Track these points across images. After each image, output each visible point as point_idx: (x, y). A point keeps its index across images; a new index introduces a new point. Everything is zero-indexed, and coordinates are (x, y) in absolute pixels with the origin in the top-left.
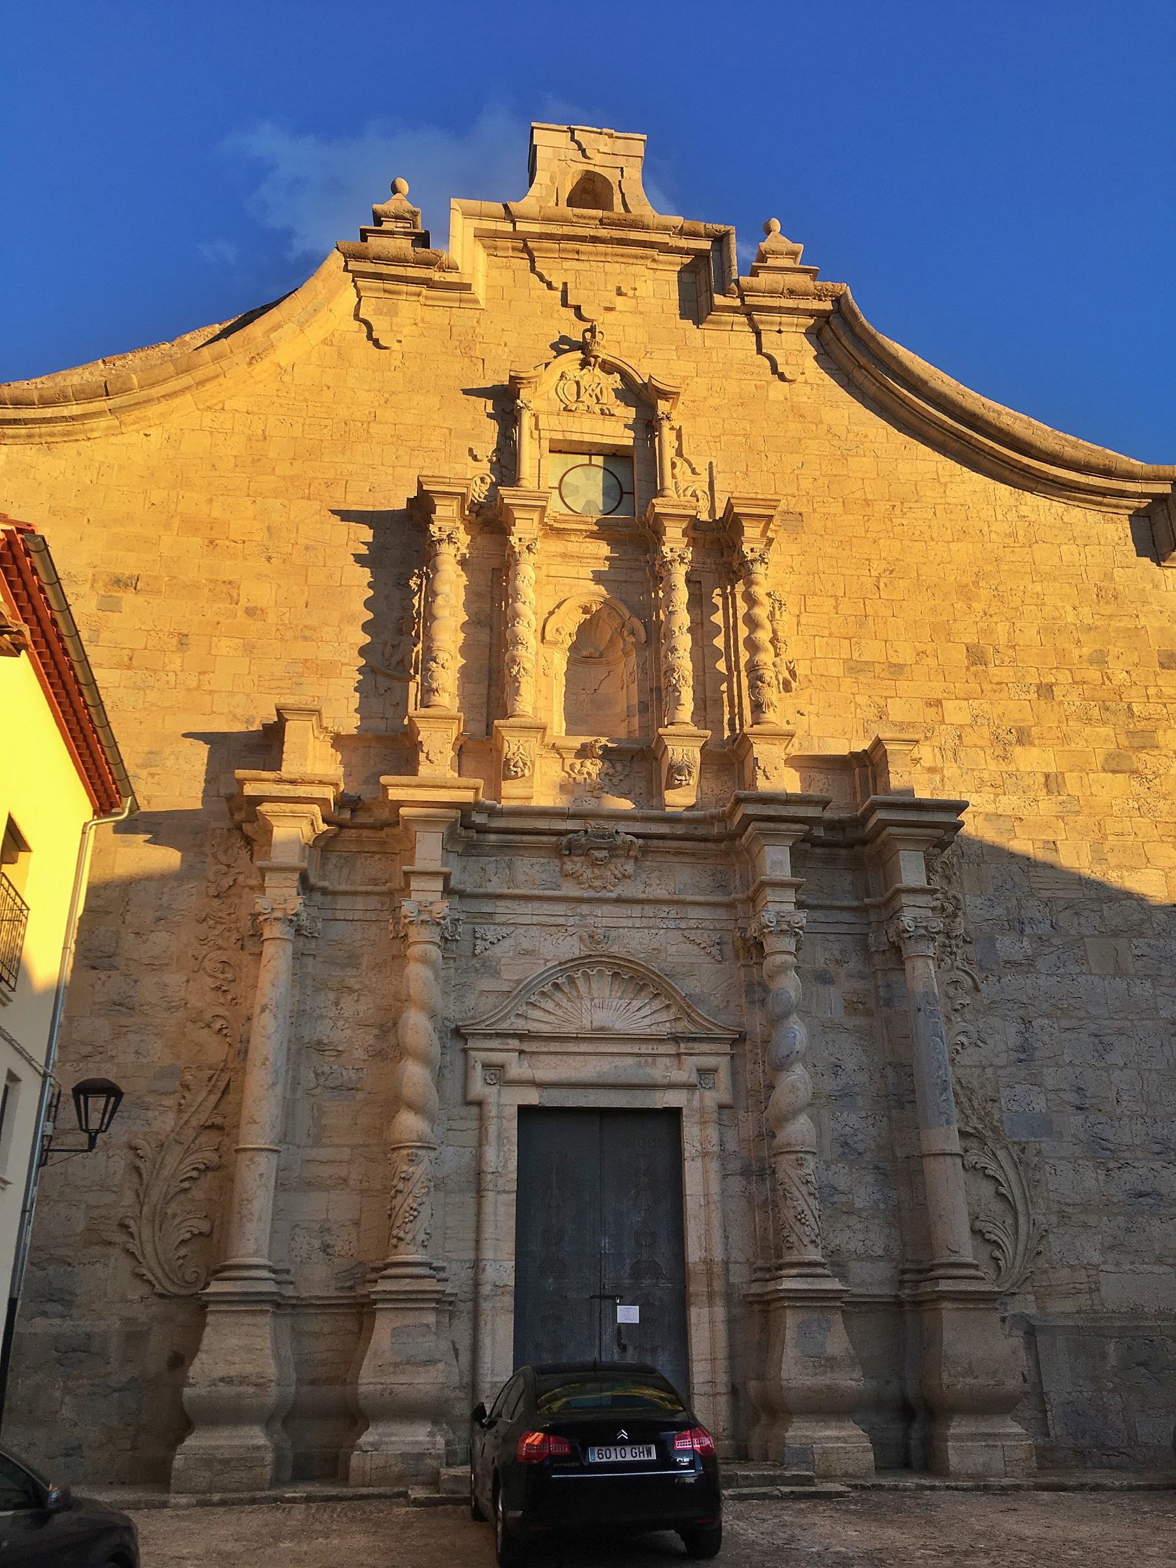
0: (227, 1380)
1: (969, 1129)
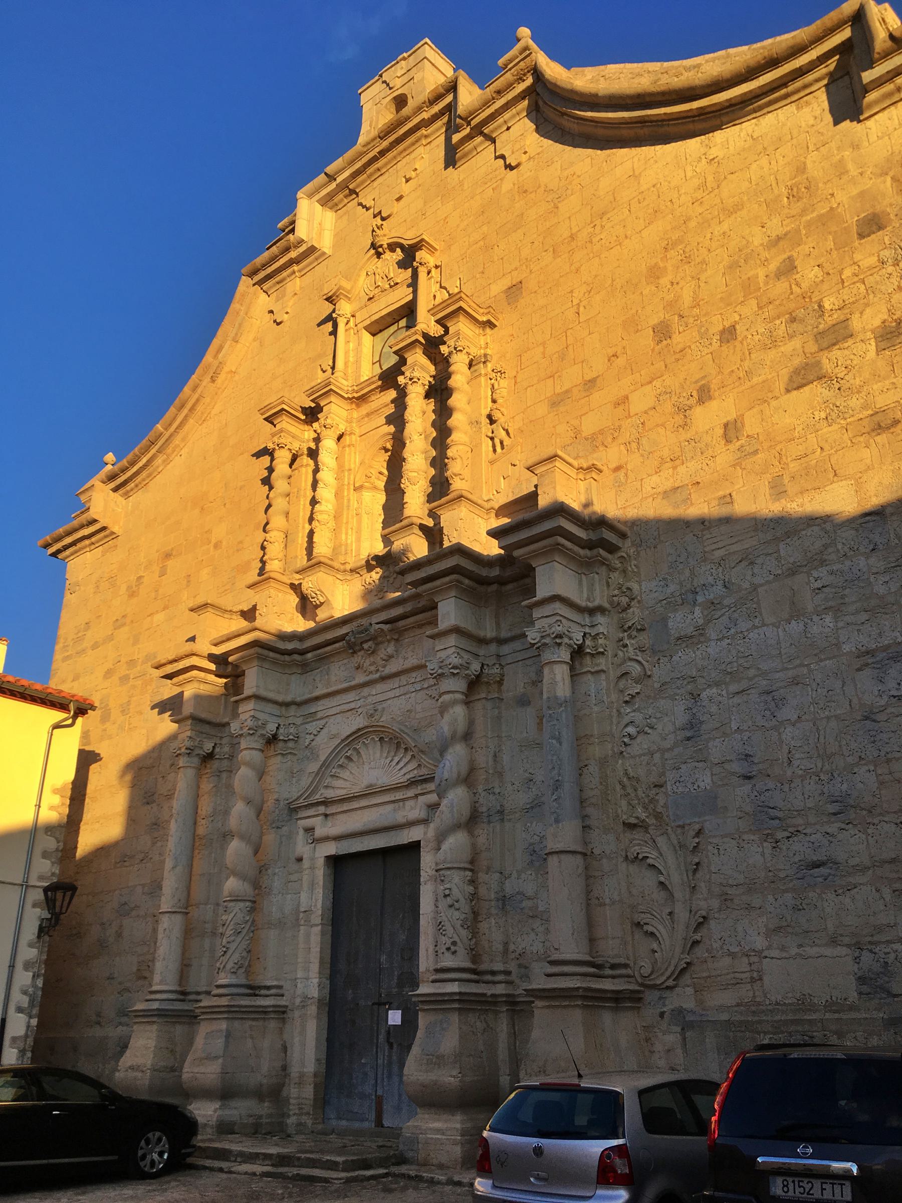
1: (633, 821)
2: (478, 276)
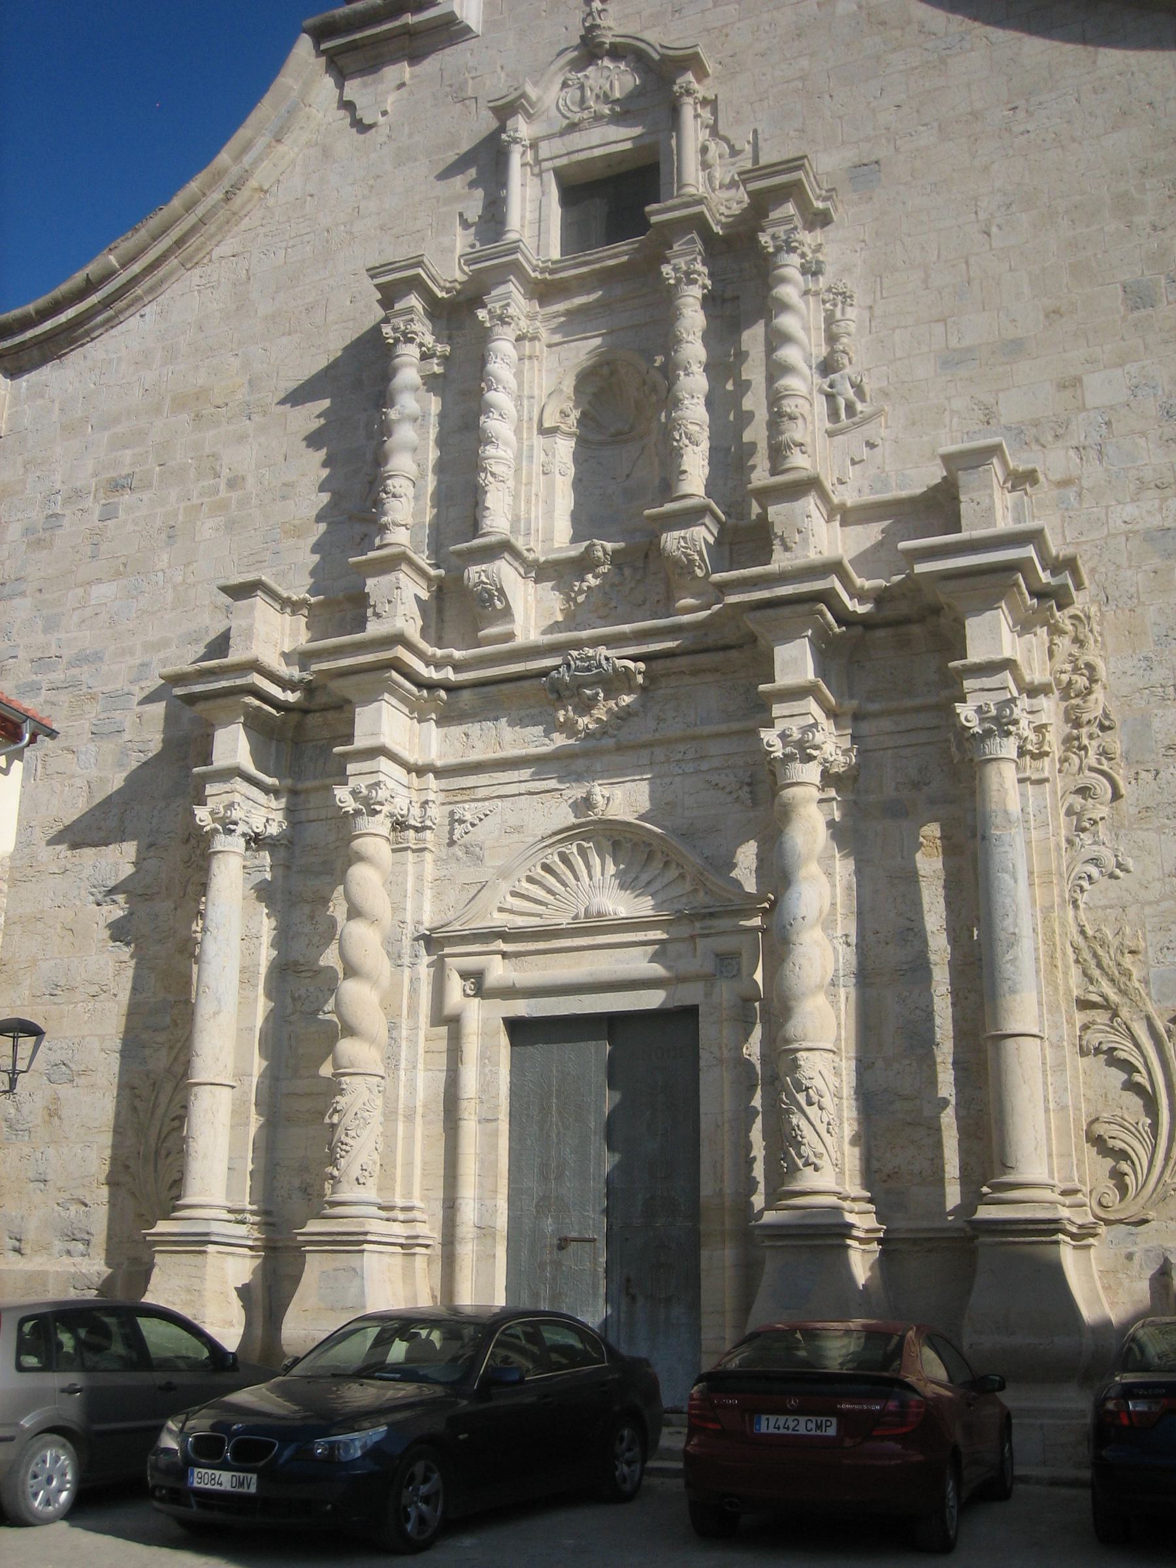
2: (792, 133)
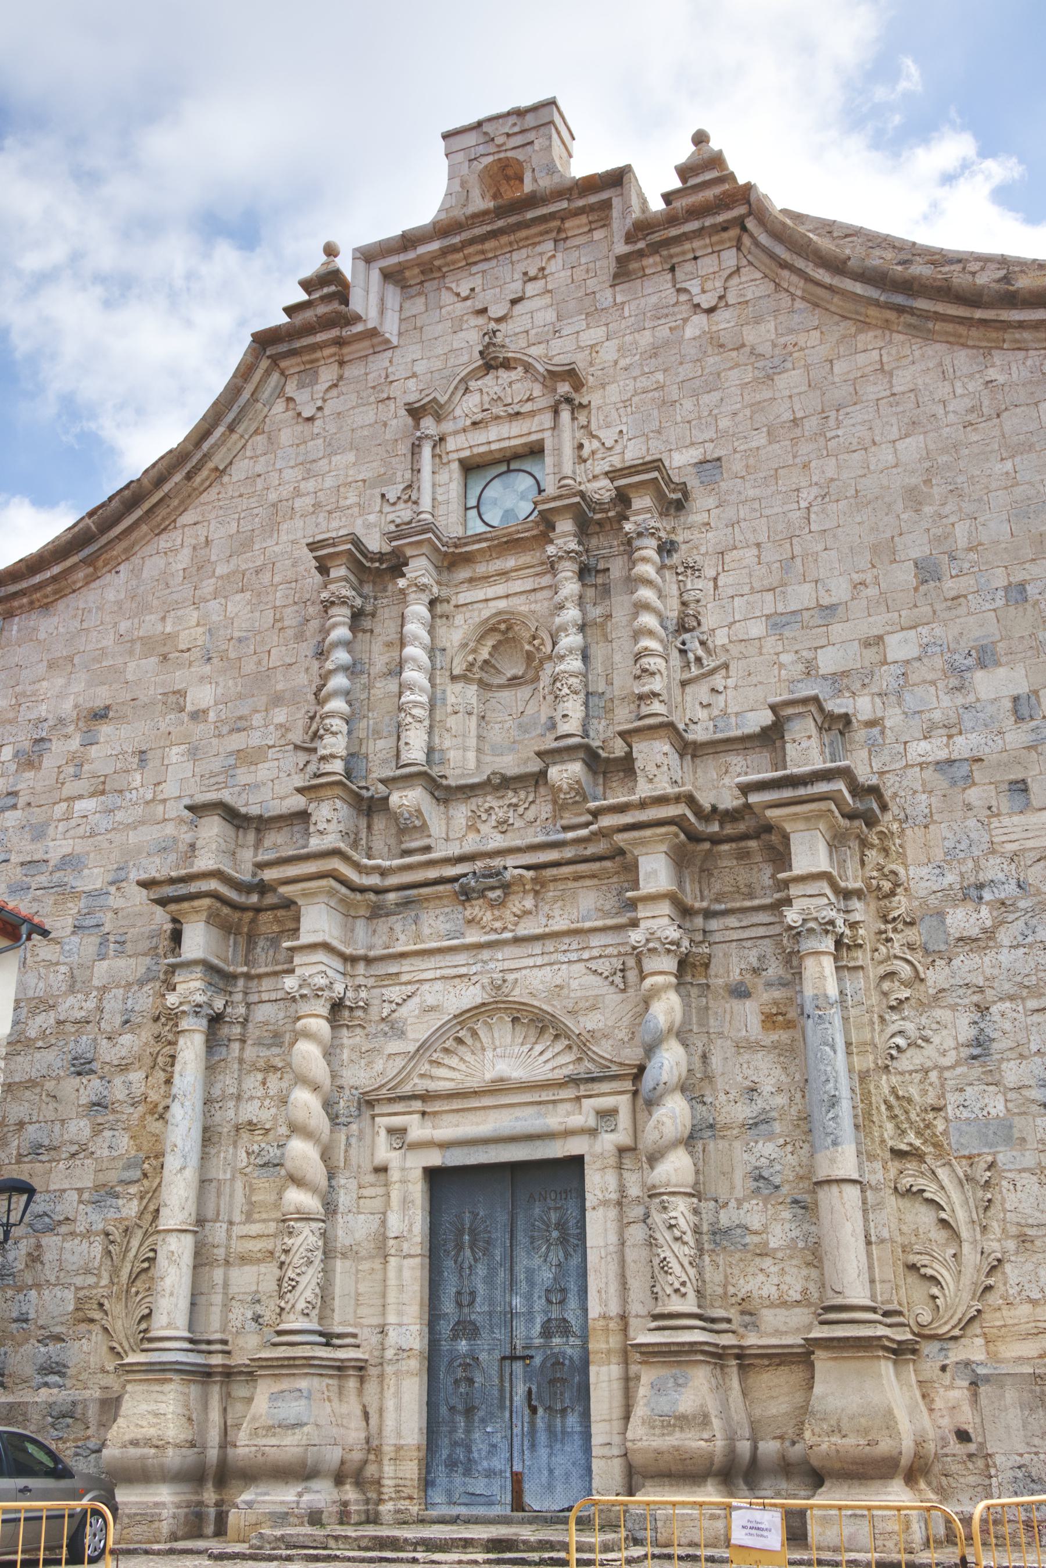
0: (134, 1443)
1: (904, 1147)
